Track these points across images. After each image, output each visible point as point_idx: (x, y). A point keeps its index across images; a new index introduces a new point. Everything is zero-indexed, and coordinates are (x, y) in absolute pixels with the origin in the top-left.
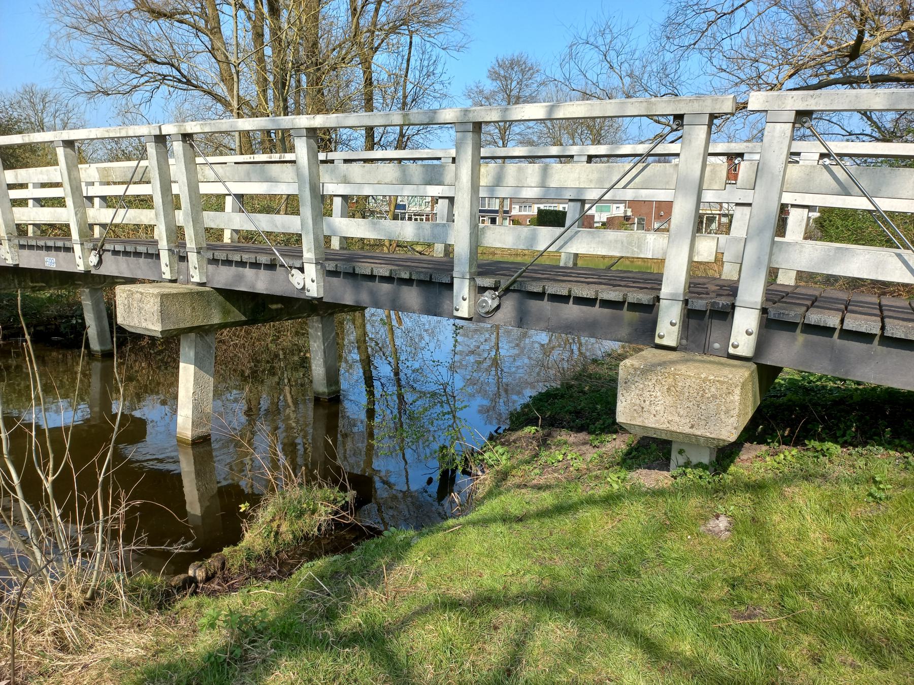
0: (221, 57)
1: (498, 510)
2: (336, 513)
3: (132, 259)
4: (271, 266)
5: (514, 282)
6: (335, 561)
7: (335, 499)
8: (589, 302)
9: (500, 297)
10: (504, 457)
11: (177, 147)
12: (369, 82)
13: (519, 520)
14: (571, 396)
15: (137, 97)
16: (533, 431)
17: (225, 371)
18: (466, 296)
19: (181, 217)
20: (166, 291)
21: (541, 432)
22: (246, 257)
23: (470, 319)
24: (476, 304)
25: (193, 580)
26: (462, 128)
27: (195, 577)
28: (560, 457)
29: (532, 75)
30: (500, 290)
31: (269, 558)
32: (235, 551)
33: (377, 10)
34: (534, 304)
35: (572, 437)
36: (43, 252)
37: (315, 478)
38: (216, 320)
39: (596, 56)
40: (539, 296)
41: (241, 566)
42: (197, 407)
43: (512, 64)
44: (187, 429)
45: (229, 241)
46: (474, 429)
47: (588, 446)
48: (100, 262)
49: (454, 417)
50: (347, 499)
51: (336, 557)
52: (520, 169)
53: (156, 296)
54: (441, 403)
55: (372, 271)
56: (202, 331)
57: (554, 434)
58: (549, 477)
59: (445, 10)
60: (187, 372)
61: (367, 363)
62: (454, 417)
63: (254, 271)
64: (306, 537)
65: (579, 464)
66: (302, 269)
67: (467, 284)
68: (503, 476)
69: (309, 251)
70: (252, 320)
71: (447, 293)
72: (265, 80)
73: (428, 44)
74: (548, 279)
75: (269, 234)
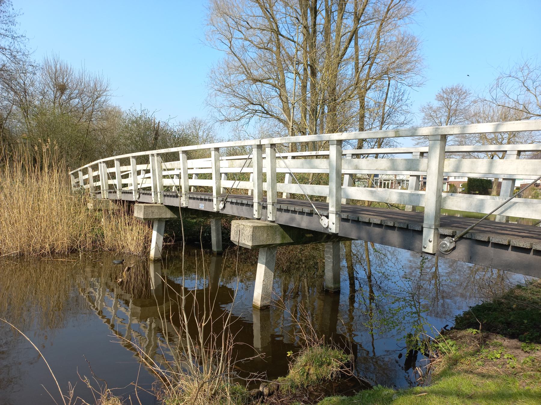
0: (284, 99)
1: (453, 387)
2: (342, 367)
3: (239, 207)
4: (311, 214)
5: (467, 233)
6: (344, 400)
7: (341, 358)
8: (526, 251)
9: (456, 242)
10: (454, 348)
11: (268, 150)
12: (362, 107)
13: (470, 397)
14: (502, 311)
15: (243, 121)
16: (474, 333)
17: (282, 270)
18: (432, 239)
19: (266, 186)
20: (256, 225)
21: (480, 335)
22: (298, 208)
23: (434, 254)
24: (438, 245)
25: (261, 394)
26: (433, 138)
27: (263, 392)
28: (498, 356)
29: (466, 96)
30: (456, 237)
31: (303, 389)
32: (284, 380)
33: (370, 68)
34: (481, 249)
35: (507, 342)
36: (199, 201)
37: (329, 342)
38: (278, 241)
39: (516, 84)
40: (486, 243)
41: (288, 390)
42: (265, 288)
43: (452, 91)
44: (258, 300)
45: (285, 197)
46: (432, 327)
47: (520, 351)
48: (224, 207)
49: (419, 316)
50: (349, 359)
51: (344, 397)
52: (472, 162)
53: (251, 227)
54: (411, 306)
55: (369, 220)
56: (270, 247)
57: (492, 337)
58: (491, 369)
59: (411, 64)
60: (261, 269)
61: (351, 269)
62: (419, 316)
63: (301, 216)
64: (324, 380)
65: (513, 363)
66: (327, 217)
67: (433, 232)
68: (454, 362)
69: (332, 206)
70: (298, 242)
71: (418, 236)
72: (306, 109)
73: (399, 84)
74: (490, 232)
75: (312, 197)
